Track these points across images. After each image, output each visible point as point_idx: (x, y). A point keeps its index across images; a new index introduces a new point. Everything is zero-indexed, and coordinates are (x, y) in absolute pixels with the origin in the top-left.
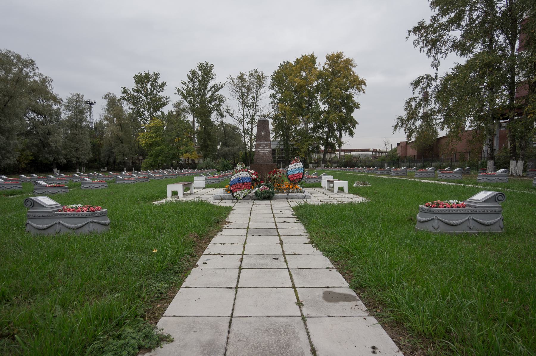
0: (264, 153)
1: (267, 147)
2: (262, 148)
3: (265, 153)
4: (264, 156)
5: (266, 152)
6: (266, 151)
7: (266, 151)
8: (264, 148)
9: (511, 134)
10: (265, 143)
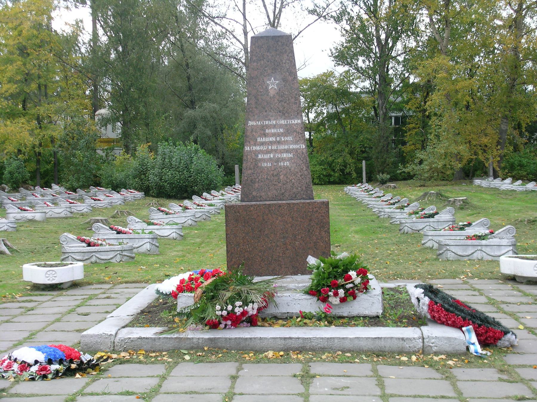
0: (278, 160)
1: (289, 138)
2: (271, 143)
3: (283, 160)
4: (278, 175)
5: (284, 155)
6: (287, 151)
7: (287, 151)
8: (279, 143)
9: (301, 205)
10: (283, 122)
